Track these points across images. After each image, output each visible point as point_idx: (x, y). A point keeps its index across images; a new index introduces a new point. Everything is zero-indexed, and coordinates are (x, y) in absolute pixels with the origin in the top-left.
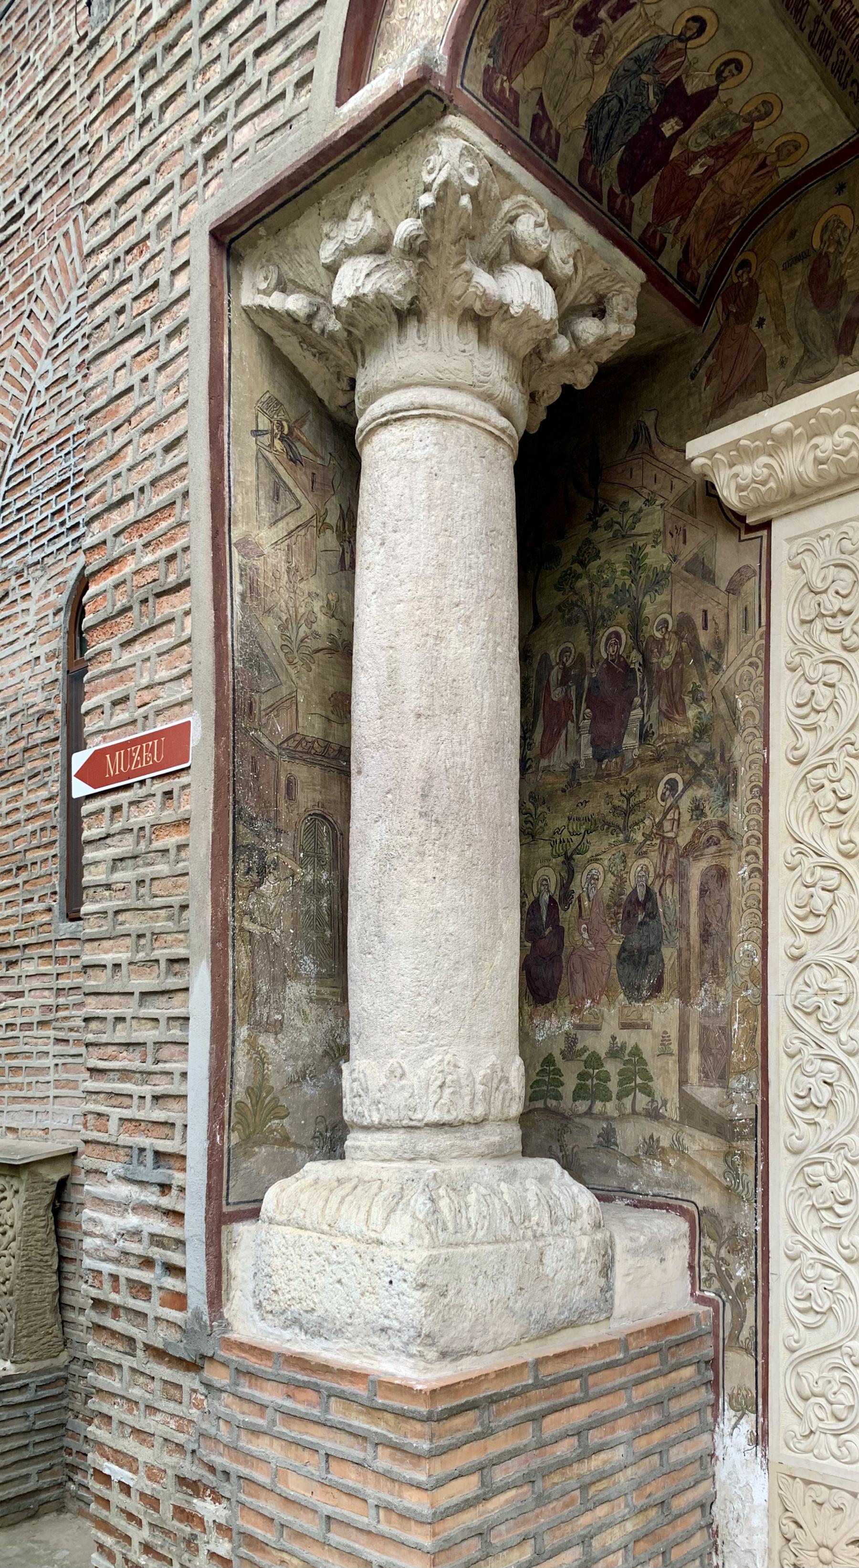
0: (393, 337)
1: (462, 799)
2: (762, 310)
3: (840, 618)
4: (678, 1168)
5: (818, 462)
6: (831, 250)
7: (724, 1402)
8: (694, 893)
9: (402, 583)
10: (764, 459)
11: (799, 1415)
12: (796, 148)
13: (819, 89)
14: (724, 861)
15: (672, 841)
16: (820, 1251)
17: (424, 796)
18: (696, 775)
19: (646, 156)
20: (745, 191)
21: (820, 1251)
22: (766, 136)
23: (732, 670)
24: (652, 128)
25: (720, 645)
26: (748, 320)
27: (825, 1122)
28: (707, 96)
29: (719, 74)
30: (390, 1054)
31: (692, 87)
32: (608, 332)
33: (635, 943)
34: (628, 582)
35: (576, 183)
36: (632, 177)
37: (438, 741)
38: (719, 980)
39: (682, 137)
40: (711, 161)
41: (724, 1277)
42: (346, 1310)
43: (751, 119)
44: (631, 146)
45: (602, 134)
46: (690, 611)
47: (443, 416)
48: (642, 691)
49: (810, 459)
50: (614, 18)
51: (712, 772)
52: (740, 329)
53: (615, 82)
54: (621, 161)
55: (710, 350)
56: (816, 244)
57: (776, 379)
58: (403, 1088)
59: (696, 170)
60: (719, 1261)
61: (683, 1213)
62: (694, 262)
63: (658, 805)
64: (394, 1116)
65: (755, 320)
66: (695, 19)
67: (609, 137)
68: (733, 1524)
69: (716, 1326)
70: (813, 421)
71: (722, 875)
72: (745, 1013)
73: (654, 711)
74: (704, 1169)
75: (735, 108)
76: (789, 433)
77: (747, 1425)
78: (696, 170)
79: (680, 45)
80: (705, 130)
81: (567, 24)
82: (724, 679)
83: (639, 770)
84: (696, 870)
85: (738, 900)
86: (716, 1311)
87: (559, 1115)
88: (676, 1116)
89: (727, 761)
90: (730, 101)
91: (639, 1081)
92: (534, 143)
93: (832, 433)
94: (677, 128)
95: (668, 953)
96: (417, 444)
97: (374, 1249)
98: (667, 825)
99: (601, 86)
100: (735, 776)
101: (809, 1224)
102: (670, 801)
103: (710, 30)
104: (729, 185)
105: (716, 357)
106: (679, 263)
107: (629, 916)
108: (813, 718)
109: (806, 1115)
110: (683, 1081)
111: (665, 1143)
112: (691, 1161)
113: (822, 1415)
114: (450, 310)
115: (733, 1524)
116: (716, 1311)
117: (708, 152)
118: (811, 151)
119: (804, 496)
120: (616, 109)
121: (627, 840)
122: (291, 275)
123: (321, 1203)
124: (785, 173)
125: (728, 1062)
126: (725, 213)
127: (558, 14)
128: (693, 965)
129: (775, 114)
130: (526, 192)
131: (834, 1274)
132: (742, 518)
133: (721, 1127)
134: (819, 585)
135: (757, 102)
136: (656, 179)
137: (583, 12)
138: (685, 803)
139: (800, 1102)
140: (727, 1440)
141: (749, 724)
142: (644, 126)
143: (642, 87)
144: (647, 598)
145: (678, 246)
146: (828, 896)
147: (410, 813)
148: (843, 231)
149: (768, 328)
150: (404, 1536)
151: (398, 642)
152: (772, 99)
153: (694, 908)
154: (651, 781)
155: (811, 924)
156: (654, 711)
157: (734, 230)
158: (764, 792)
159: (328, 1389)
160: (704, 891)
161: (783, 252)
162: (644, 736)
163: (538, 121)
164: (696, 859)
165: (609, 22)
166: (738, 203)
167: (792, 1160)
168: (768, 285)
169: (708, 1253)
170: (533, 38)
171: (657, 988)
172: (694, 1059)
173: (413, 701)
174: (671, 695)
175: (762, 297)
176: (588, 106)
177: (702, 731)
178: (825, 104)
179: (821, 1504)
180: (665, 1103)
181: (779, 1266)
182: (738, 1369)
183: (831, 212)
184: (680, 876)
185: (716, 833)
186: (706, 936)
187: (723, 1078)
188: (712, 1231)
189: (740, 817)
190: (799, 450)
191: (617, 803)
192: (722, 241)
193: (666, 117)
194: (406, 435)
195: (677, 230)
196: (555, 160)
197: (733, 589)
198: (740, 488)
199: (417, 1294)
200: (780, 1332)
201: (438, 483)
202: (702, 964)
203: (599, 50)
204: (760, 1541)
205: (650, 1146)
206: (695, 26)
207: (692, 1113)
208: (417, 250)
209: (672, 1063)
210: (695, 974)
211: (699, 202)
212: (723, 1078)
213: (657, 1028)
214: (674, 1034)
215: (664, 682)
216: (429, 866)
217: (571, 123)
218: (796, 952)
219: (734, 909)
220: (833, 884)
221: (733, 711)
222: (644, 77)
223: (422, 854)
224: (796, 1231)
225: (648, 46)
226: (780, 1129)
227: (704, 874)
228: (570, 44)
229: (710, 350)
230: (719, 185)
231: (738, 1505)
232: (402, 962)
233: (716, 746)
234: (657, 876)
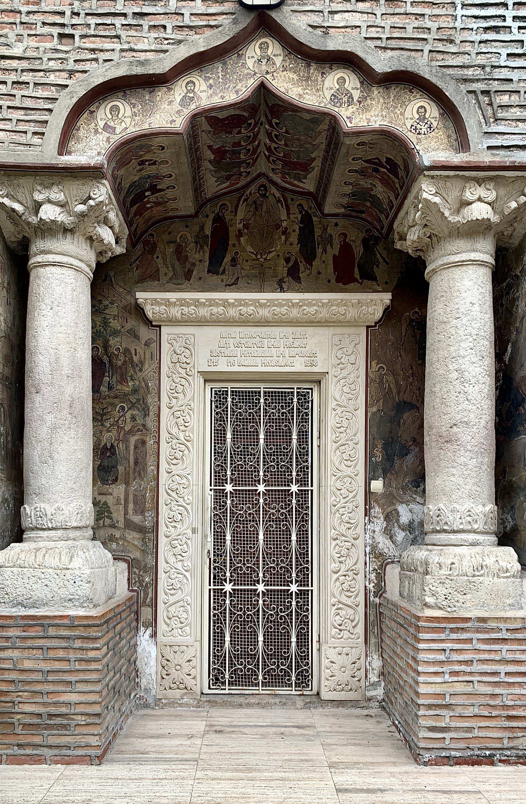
0: (60, 236)
1: (83, 410)
3: (185, 364)
4: (123, 545)
7: (140, 625)
8: (132, 448)
9: (61, 326)
11: (168, 625)
14: (144, 438)
15: (123, 428)
16: (176, 569)
17: (71, 407)
18: (133, 406)
19: (139, 198)
21: (176, 569)
22: (171, 205)
23: (146, 372)
24: (143, 192)
25: (142, 363)
26: (153, 254)
27: (178, 527)
30: (56, 502)
32: (119, 250)
33: (106, 463)
34: (102, 330)
36: (133, 203)
37: (75, 387)
38: (142, 479)
41: (141, 582)
42: (49, 596)
43: (170, 199)
44: (136, 194)
46: (130, 348)
47: (77, 270)
48: (109, 371)
51: (139, 406)
57: (164, 279)
58: (63, 514)
59: (148, 206)
60: (139, 576)
61: (125, 560)
63: (116, 414)
64: (59, 525)
68: (144, 666)
69: (138, 599)
71: (144, 442)
72: (151, 490)
73: (114, 379)
74: (133, 544)
75: (167, 196)
77: (149, 631)
78: (148, 206)
80: (156, 197)
82: (144, 374)
83: (108, 400)
84: (133, 440)
85: (150, 452)
86: (138, 594)
87: (103, 525)
88: (123, 526)
89: (145, 404)
91: (106, 514)
92: (117, 190)
95: (121, 469)
96: (67, 277)
97: (66, 571)
98: (120, 422)
99: (136, 178)
100: (149, 409)
101: (172, 560)
102: (121, 414)
104: (154, 212)
107: (102, 453)
108: (176, 395)
109: (171, 524)
110: (126, 513)
111: (117, 536)
112: (128, 542)
113: (176, 623)
114: (84, 235)
115: (144, 666)
116: (138, 594)
119: (175, 322)
121: (102, 425)
122: (12, 193)
123: (33, 557)
124: (170, 214)
125: (145, 507)
126: (150, 218)
128: (131, 473)
130: (113, 205)
131: (181, 576)
132: (151, 322)
133: (141, 529)
134: (179, 352)
138: (128, 415)
139: (170, 520)
140: (142, 638)
141: (154, 392)
142: (142, 191)
144: (111, 338)
146: (181, 453)
147: (65, 412)
150: (89, 668)
151: (60, 348)
153: (132, 452)
154: (114, 405)
155: (175, 461)
156: (114, 379)
158: (159, 416)
159: (48, 624)
160: (136, 447)
162: (110, 388)
163: (120, 183)
164: (133, 435)
167: (166, 539)
168: (160, 246)
169: (135, 573)
171: (115, 480)
172: (131, 506)
173: (66, 371)
174: (122, 375)
175: (158, 249)
177: (135, 391)
178: (191, 204)
179: (176, 652)
180: (118, 522)
181: (161, 575)
182: (146, 613)
184: (126, 441)
185: (141, 427)
186: (136, 463)
187: (142, 512)
188: (137, 566)
189: (150, 422)
191: (97, 410)
194: (63, 272)
197: (147, 344)
198: (153, 313)
199: (87, 585)
200: (161, 597)
201: (75, 293)
202: (135, 473)
203: (141, 170)
204: (153, 670)
205: (111, 538)
207: (129, 525)
208: (82, 215)
209: (121, 508)
210: (131, 475)
212: (142, 512)
213: (115, 495)
214: (122, 497)
215: (119, 370)
216: (72, 433)
217: (126, 185)
218: (170, 471)
219: (148, 455)
220: (183, 449)
221: (147, 386)
223: (70, 428)
224: (167, 563)
226: (162, 529)
227: (136, 441)
230: (152, 211)
231: (146, 659)
232: (62, 468)
233: (141, 397)
234: (116, 440)
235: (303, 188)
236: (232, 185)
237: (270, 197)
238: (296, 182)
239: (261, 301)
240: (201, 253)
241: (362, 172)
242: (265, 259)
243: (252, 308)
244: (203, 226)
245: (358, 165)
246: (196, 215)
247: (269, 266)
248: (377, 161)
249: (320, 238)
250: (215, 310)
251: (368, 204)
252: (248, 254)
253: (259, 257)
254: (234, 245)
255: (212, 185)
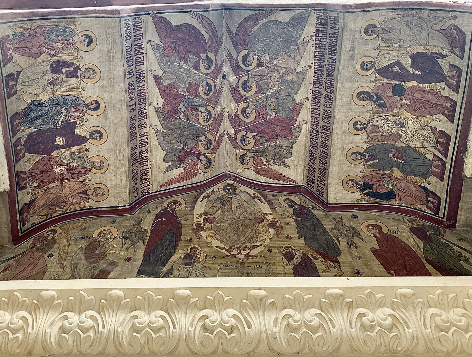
2: (54, 250)
5: (63, 330)
6: (103, 240)
10: (24, 313)
12: (102, 195)
13: (125, 172)
20: (71, 199)
22: (94, 179)
28: (81, 140)
29: (92, 134)
31: (79, 131)
35: (9, 117)
39: (61, 150)
40: (66, 172)
45: (32, 115)
49: (58, 325)
50: (67, 76)
52: (37, 254)
53: (51, 100)
54: (31, 134)
55: (14, 257)
56: (95, 235)
59: (58, 170)
62: (31, 211)
65: (48, 254)
66: (97, 102)
67: (34, 119)
70: (72, 298)
75: (89, 155)
76: (52, 299)
79: (85, 109)
80: (72, 155)
81: (49, 61)
90: (88, 150)
93: (80, 314)
94: (62, 143)
103: (100, 111)
104: (66, 190)
105: (16, 262)
106: (26, 204)
117: (67, 166)
118: (107, 200)
120: (44, 112)
124: (91, 204)
127: (49, 54)
129: (103, 171)
135: (99, 159)
136: (40, 157)
137: (58, 62)
143: (59, 113)
145: (30, 196)
148: (111, 236)
149: (54, 259)
152: (106, 163)
157: (56, 214)
161: (77, 233)
165: (65, 76)
166: (64, 202)
168: (63, 242)
170: (33, 51)
175: (56, 246)
176: (35, 98)
183: (107, 228)
190: (53, 316)
192: (48, 214)
193: (61, 135)
195: (33, 189)
196: (8, 98)
203: (53, 83)
206: (95, 105)
211: (50, 186)
222: (63, 110)
225: (73, 98)
228: (45, 69)
229: (14, 257)
230: (62, 186)
235: (288, 179)
236: (187, 175)
237: (241, 195)
238: (276, 168)
239: (252, 292)
240: (132, 250)
241: (376, 98)
242: (247, 255)
243: (232, 312)
244: (140, 221)
245: (370, 82)
246: (132, 208)
247: (257, 264)
248: (397, 69)
249: (335, 231)
250: (143, 317)
251: (397, 173)
252: (215, 250)
253: (234, 252)
254: (190, 240)
255: (161, 172)
